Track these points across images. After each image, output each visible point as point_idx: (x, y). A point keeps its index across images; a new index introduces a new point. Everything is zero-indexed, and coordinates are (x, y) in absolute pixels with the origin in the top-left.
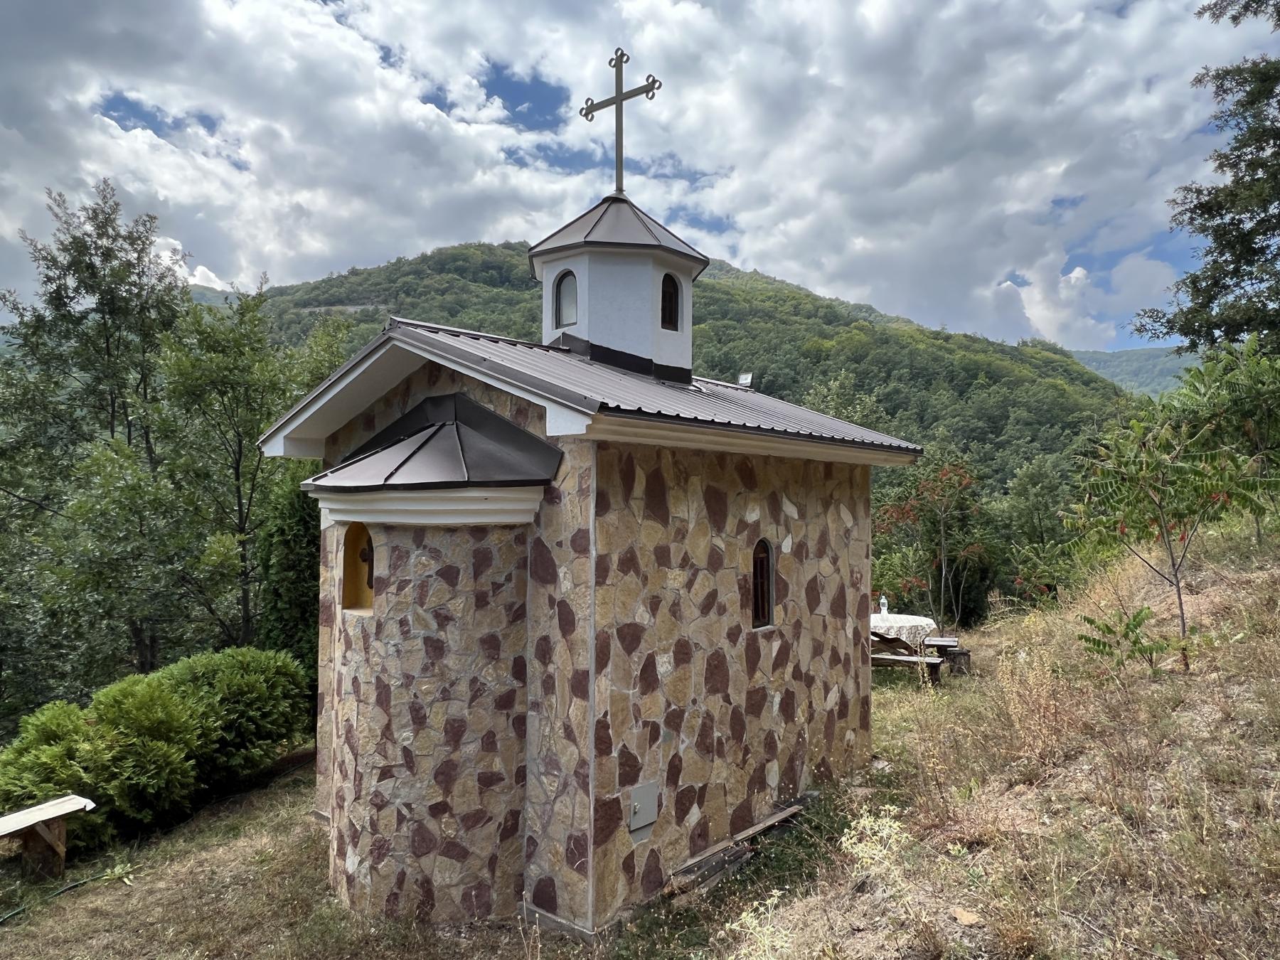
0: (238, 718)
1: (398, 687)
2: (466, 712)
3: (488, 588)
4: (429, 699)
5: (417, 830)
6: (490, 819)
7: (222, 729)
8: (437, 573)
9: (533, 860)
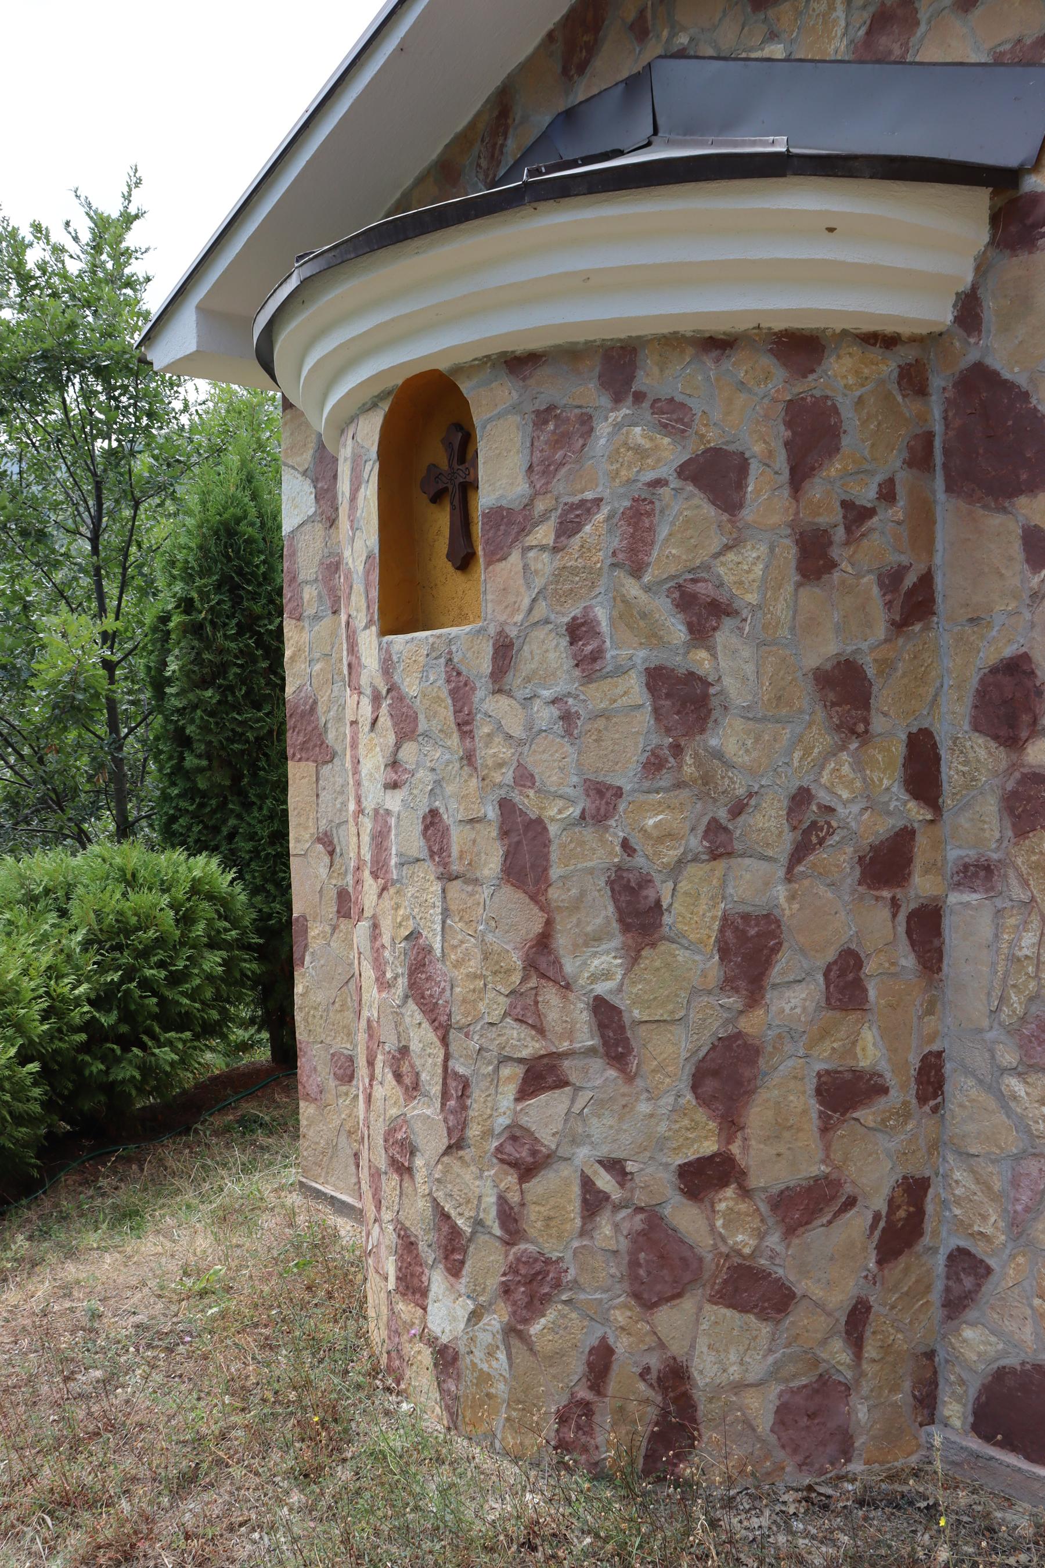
0: (122, 981)
1: (569, 825)
2: (781, 892)
3: (832, 517)
4: (671, 854)
5: (642, 1233)
6: (851, 1202)
7: (90, 1002)
8: (683, 472)
9: (971, 1314)
